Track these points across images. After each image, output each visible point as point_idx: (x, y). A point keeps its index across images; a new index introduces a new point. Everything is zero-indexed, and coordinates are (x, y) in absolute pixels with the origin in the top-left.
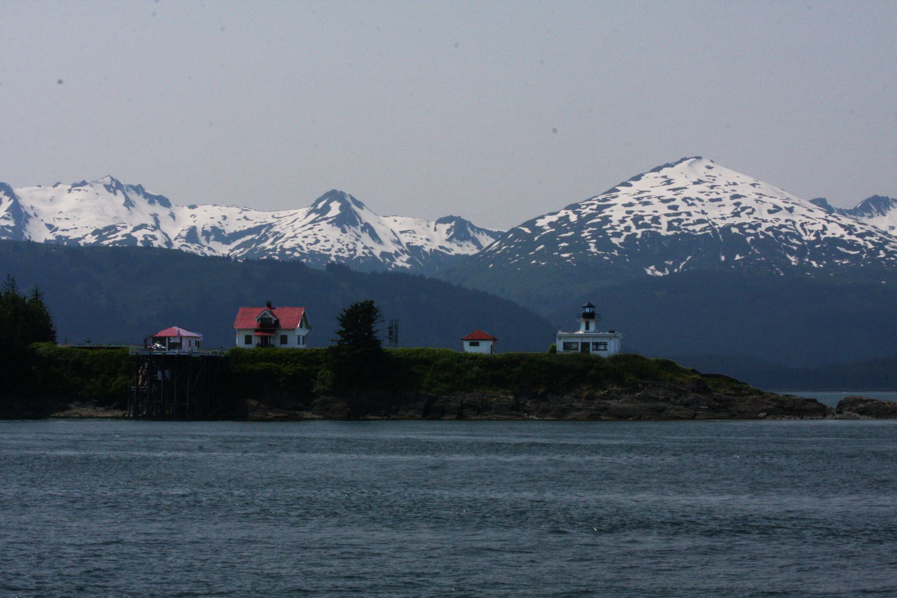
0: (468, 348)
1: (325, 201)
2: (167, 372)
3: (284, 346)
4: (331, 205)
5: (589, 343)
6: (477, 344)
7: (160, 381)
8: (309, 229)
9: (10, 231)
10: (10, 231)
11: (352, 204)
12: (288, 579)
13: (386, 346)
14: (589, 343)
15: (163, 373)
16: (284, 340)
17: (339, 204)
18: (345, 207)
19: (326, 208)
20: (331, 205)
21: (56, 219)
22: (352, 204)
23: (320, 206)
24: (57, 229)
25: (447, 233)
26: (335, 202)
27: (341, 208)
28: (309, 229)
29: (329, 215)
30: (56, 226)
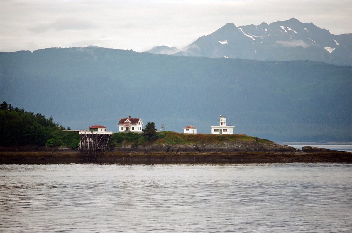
15: (89, 139)
16: (133, 129)
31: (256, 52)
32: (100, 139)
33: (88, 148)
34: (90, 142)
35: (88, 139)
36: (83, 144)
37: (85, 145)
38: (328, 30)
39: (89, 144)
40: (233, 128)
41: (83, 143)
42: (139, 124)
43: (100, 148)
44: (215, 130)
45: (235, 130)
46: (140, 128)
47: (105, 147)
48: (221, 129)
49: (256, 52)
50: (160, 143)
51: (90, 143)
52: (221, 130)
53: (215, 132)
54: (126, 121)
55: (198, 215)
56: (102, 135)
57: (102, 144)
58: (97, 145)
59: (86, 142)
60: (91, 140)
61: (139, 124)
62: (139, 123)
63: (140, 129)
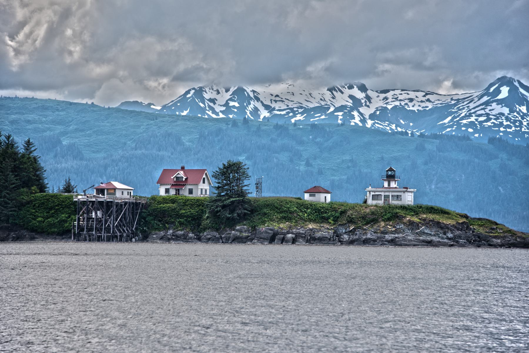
0: (307, 196)
1: (497, 85)
2: (98, 212)
3: (191, 195)
4: (501, 89)
5: (389, 195)
6: (314, 196)
7: (94, 219)
8: (482, 109)
9: (236, 110)
10: (236, 110)
11: (520, 88)
12: (273, 307)
13: (252, 194)
14: (389, 195)
15: (96, 213)
16: (191, 192)
17: (508, 88)
18: (513, 90)
19: (498, 91)
20: (501, 89)
21: (273, 101)
22: (520, 88)
23: (492, 90)
24: (274, 109)
25: (350, 95)
26: (505, 87)
27: (509, 91)
28: (482, 109)
29: (500, 97)
30: (273, 107)
31: (173, 108)
32: (122, 212)
33: (94, 232)
34: (97, 219)
35: (94, 214)
36: (84, 223)
37: (87, 226)
38: (365, 84)
39: (96, 225)
40: (413, 194)
41: (83, 221)
42: (204, 182)
43: (120, 232)
44: (375, 197)
45: (415, 198)
46: (206, 190)
47: (132, 230)
48: (387, 194)
49: (173, 108)
50: (296, 231)
51: (99, 221)
52: (387, 197)
53: (373, 201)
54: (175, 175)
55: (211, 336)
56: (126, 203)
57: (124, 225)
58: (113, 226)
59: (90, 218)
60: (99, 214)
61: (204, 182)
62: (204, 179)
63: (202, 190)
